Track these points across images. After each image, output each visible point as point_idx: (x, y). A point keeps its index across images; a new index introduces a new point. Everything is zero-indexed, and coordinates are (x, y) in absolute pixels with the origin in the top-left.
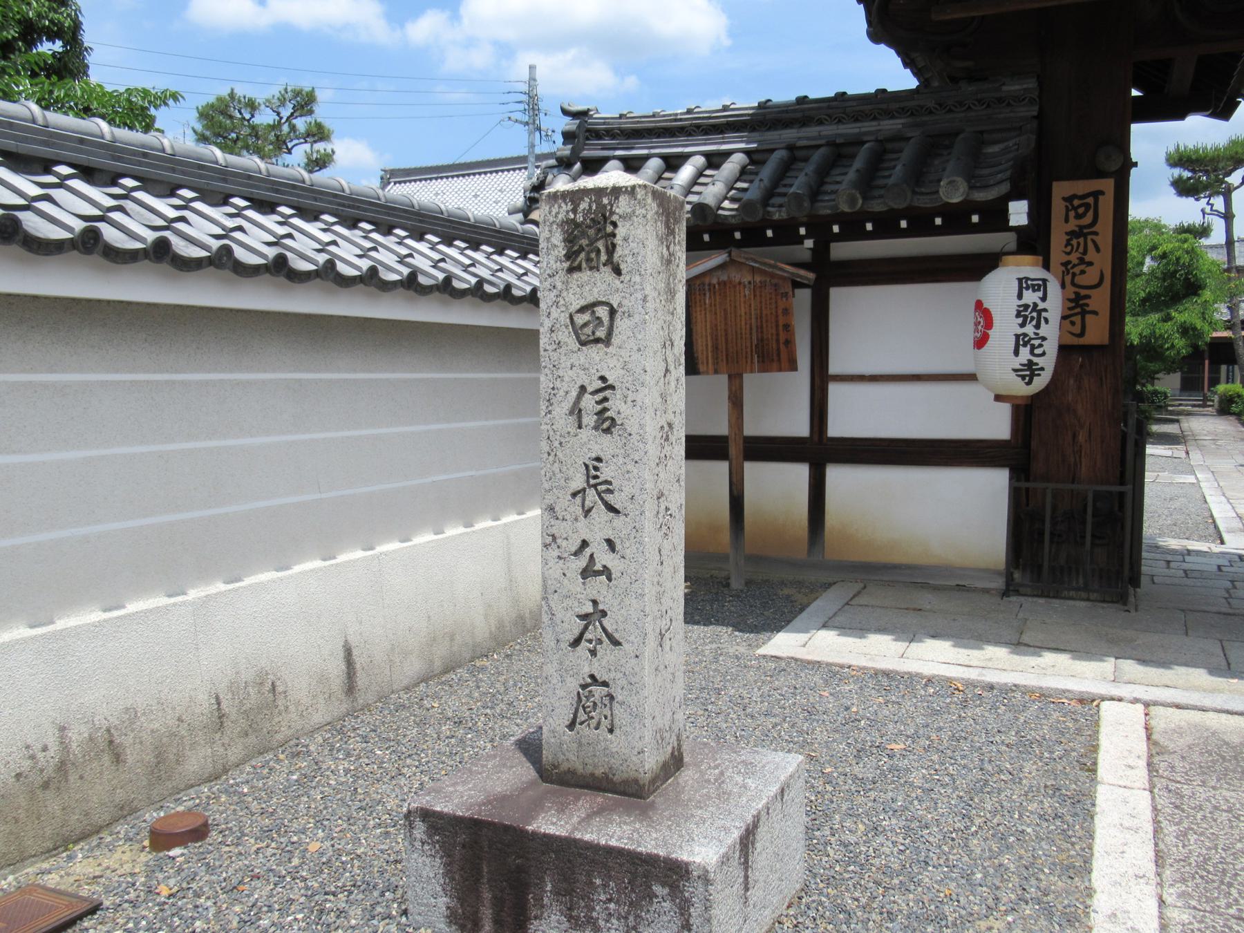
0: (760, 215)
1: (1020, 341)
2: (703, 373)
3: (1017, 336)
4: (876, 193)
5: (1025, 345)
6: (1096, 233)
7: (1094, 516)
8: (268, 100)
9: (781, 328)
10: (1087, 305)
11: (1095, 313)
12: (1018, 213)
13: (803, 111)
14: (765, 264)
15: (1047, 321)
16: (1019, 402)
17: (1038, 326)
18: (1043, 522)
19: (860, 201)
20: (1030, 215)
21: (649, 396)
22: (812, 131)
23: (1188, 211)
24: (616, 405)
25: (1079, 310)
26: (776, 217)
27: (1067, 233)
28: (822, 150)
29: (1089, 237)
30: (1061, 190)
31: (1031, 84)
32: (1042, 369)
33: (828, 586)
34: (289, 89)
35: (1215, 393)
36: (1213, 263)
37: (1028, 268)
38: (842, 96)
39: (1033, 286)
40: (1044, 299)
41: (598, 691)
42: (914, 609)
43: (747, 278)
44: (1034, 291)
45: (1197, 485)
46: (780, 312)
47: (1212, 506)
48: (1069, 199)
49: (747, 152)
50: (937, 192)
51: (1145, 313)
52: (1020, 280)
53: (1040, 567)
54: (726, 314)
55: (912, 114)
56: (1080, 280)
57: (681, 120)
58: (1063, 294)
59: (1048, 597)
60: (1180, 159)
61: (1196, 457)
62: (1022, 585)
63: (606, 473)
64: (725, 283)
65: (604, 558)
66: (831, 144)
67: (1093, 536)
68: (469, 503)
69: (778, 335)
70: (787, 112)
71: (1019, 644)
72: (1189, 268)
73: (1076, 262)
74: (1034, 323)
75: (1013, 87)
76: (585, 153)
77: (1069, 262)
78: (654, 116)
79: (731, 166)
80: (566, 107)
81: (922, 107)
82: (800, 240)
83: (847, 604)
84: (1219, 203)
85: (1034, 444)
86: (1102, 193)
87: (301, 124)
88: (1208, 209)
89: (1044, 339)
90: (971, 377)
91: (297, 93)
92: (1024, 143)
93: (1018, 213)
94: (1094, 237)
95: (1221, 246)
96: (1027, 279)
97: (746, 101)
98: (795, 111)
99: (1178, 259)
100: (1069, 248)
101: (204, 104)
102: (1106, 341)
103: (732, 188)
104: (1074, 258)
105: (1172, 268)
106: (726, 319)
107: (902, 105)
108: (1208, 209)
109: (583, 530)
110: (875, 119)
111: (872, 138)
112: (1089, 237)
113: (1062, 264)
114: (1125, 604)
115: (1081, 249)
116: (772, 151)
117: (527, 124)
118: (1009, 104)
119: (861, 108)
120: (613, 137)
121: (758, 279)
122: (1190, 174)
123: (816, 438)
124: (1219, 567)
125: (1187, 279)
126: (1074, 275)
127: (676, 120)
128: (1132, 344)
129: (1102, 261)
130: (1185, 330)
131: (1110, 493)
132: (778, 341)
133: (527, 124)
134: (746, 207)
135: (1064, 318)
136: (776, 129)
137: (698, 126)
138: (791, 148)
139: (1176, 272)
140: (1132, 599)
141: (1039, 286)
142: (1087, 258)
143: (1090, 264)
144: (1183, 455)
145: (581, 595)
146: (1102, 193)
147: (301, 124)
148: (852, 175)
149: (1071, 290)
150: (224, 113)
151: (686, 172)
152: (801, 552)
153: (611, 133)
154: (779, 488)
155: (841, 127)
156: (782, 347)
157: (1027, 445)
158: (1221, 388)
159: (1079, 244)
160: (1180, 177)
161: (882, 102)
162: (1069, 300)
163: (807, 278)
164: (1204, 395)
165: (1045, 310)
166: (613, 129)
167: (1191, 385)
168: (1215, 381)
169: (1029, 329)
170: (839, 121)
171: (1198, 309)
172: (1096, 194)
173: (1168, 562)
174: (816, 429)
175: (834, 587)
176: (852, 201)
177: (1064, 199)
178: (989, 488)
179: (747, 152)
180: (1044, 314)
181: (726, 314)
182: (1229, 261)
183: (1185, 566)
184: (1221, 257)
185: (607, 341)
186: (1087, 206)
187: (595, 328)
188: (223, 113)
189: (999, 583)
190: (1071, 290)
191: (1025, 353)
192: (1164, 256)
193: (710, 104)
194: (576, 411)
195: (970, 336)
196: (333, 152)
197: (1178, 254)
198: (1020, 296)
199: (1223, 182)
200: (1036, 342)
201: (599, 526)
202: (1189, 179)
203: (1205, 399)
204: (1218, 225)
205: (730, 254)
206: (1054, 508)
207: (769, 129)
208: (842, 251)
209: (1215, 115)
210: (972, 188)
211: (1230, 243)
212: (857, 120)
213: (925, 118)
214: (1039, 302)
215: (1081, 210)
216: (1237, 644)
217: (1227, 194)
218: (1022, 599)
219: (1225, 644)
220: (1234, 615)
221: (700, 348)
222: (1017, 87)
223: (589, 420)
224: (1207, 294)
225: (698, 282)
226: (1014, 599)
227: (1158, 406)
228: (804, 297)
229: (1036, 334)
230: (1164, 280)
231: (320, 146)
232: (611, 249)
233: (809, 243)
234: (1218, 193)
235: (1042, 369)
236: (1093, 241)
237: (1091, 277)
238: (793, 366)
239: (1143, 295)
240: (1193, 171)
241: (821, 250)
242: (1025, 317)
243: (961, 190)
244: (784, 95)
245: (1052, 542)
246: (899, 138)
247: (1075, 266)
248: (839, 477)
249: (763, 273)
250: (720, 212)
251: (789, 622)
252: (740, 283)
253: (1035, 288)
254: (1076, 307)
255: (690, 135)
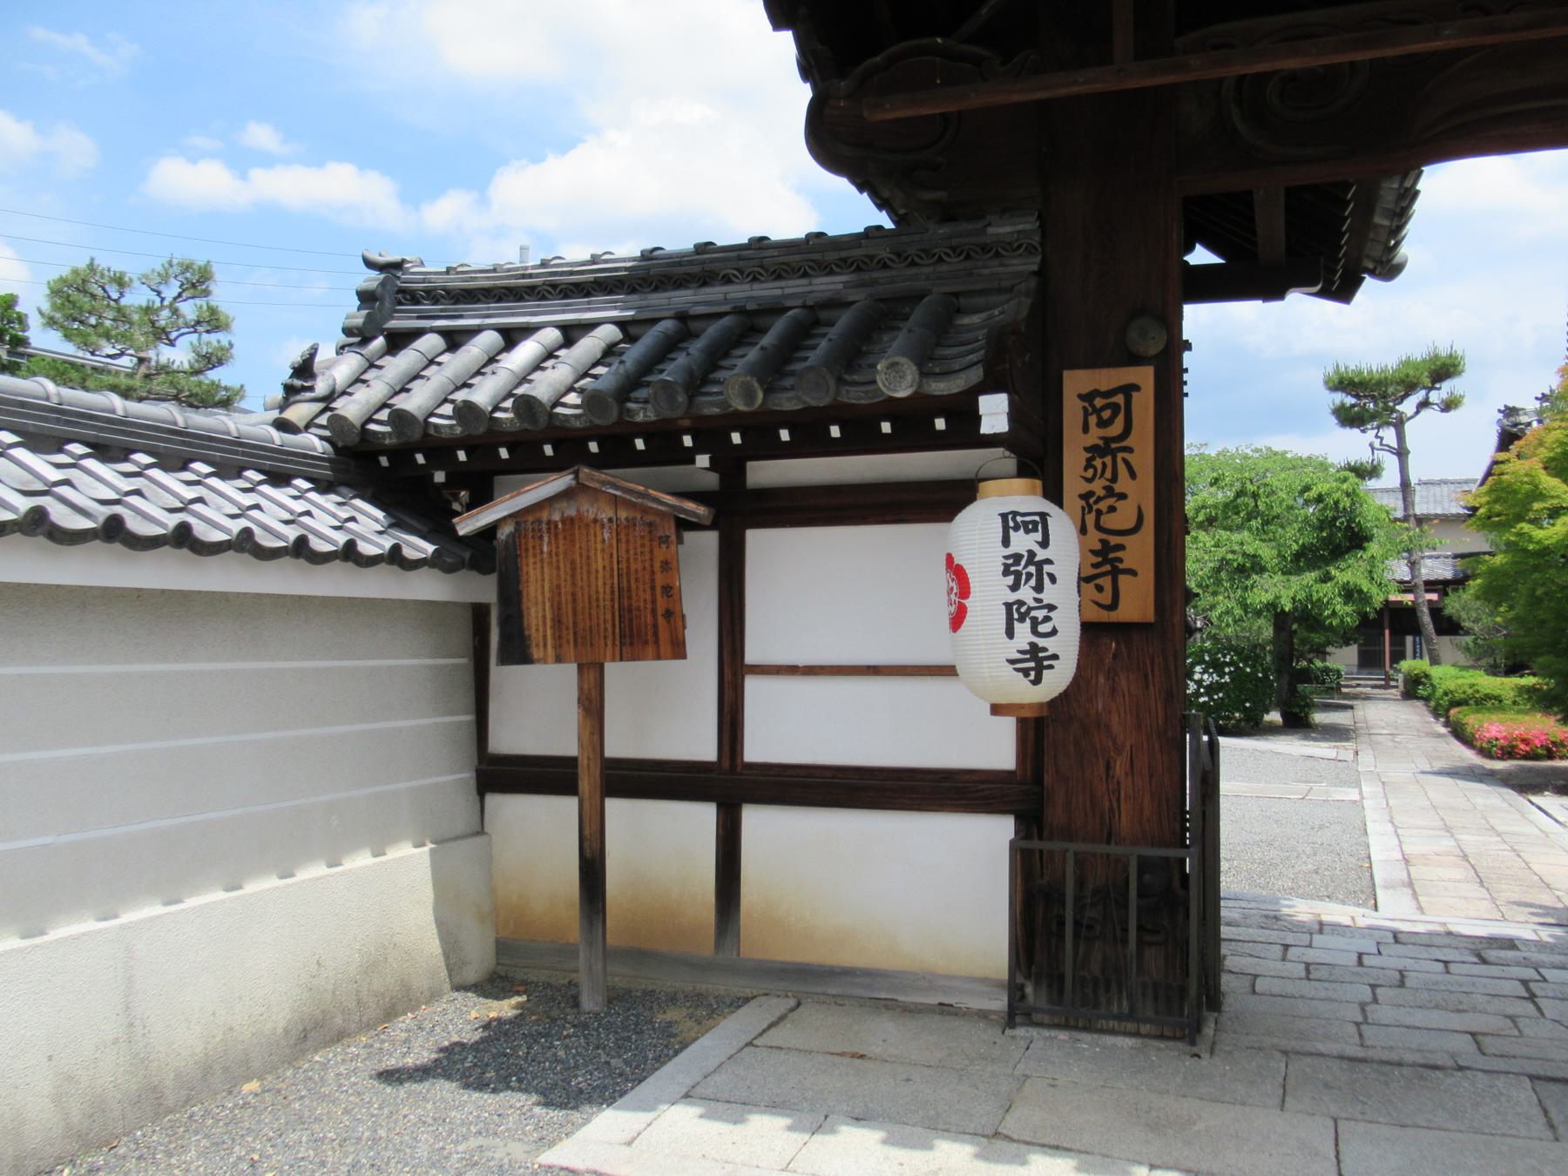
0: (614, 415)
1: (1014, 613)
2: (539, 661)
3: (1008, 606)
4: (788, 382)
5: (1022, 619)
6: (1129, 450)
7: (1140, 895)
8: (146, 276)
9: (658, 591)
10: (1120, 560)
11: (1133, 573)
12: (994, 413)
13: (703, 262)
14: (630, 492)
15: (1053, 579)
16: (1027, 714)
17: (1039, 588)
18: (1063, 904)
19: (760, 395)
20: (1013, 416)
22: (715, 292)
23: (1354, 445)
25: (1108, 567)
26: (640, 418)
27: (1086, 449)
28: (726, 321)
29: (1120, 455)
30: (1076, 382)
31: (1028, 224)
32: (1055, 657)
33: (740, 1002)
34: (175, 262)
35: (1399, 671)
36: (1381, 508)
37: (1018, 498)
38: (760, 243)
39: (1025, 524)
40: (1044, 544)
42: (853, 1056)
43: (606, 514)
44: (1027, 531)
45: (1358, 805)
46: (657, 565)
47: (1372, 840)
48: (1088, 397)
49: (621, 324)
50: (875, 382)
51: (1298, 571)
52: (1004, 516)
53: (1061, 977)
54: (573, 569)
55: (859, 269)
56: (1109, 521)
57: (530, 276)
58: (1081, 544)
59: (1076, 1028)
60: (1341, 382)
61: (1366, 758)
62: (1038, 1010)
64: (572, 520)
66: (739, 311)
67: (1140, 928)
68: (281, 847)
69: (654, 601)
70: (680, 264)
71: (996, 1134)
72: (1351, 514)
73: (1101, 493)
74: (1033, 582)
75: (1002, 229)
76: (393, 324)
77: (1090, 494)
78: (494, 270)
79: (590, 345)
80: (374, 256)
81: (871, 258)
82: (688, 457)
83: (750, 1044)
84: (1389, 435)
85: (1048, 779)
86: (1137, 388)
87: (189, 309)
88: (1377, 443)
89: (1051, 608)
90: (948, 671)
91: (187, 268)
92: (1012, 309)
93: (994, 413)
94: (1126, 455)
95: (1393, 490)
96: (1015, 514)
97: (626, 250)
98: (690, 263)
99: (1336, 503)
100: (1090, 473)
101: (57, 277)
102: (1150, 617)
103: (586, 375)
104: (1098, 487)
105: (1330, 514)
106: (573, 576)
107: (844, 254)
108: (1377, 443)
110: (805, 275)
111: (799, 302)
112: (1120, 455)
113: (1081, 496)
114: (1193, 1043)
115: (1108, 474)
116: (654, 321)
118: (998, 255)
119: (786, 259)
120: (436, 301)
121: (623, 514)
122: (1353, 401)
123: (726, 764)
124: (1360, 956)
125: (1349, 528)
126: (1099, 513)
127: (524, 276)
128: (1283, 611)
129: (1140, 492)
130: (1349, 593)
131: (1167, 859)
132: (654, 611)
134: (592, 400)
135: (1083, 580)
136: (665, 290)
137: (554, 286)
138: (682, 317)
139: (1335, 519)
140: (1209, 1030)
141: (1035, 523)
142: (1118, 488)
143: (1122, 496)
144: (1349, 756)
146: (1137, 388)
147: (189, 309)
148: (753, 354)
149: (1094, 537)
150: (82, 290)
151: (527, 350)
153: (432, 295)
154: (662, 844)
155: (756, 286)
156: (661, 620)
157: (1038, 779)
158: (1406, 665)
159: (1104, 465)
160: (1343, 405)
161: (816, 253)
162: (1093, 552)
163: (695, 514)
164: (1386, 673)
165: (1049, 562)
166: (435, 289)
167: (1370, 661)
168: (1398, 656)
169: (1026, 594)
170: (755, 279)
171: (1364, 566)
172: (1129, 390)
173: (1286, 947)
174: (726, 749)
175: (754, 1003)
176: (749, 395)
177: (1081, 397)
178: (989, 838)
179: (621, 324)
180: (1047, 568)
181: (573, 569)
182: (1406, 509)
183: (1311, 955)
184: (1395, 505)
186: (1115, 408)
188: (82, 290)
189: (1000, 1003)
190: (1094, 537)
191: (1023, 630)
192: (1320, 499)
193: (575, 253)
195: (945, 613)
196: (231, 345)
197: (1336, 496)
198: (1006, 542)
199: (1393, 410)
200: (1040, 614)
202: (1353, 406)
203: (1388, 679)
204: (1390, 463)
205: (576, 474)
206: (1081, 883)
207: (656, 289)
208: (764, 473)
209: (1325, 293)
210: (924, 374)
211: (1405, 485)
212: (779, 277)
213: (875, 275)
214: (1036, 548)
215: (1106, 414)
216: (1362, 1127)
217: (1399, 425)
218: (1033, 1032)
219: (1342, 1126)
220: (1364, 1061)
221: (534, 622)
222: (1008, 229)
224: (1373, 548)
225: (531, 519)
226: (1021, 1032)
227: (1330, 685)
228: (706, 544)
229: (1037, 600)
230: (1321, 529)
231: (213, 338)
233: (703, 460)
234: (1388, 424)
235: (1055, 657)
236: (1124, 460)
237: (1123, 517)
239: (1295, 547)
240: (1357, 396)
242: (1018, 575)
243: (909, 378)
244: (678, 241)
245: (1077, 936)
246: (836, 303)
247: (1099, 499)
248: (762, 825)
249: (633, 506)
250: (559, 410)
251: (623, 1094)
252: (595, 521)
253: (1029, 528)
254: (1103, 565)
255: (544, 298)
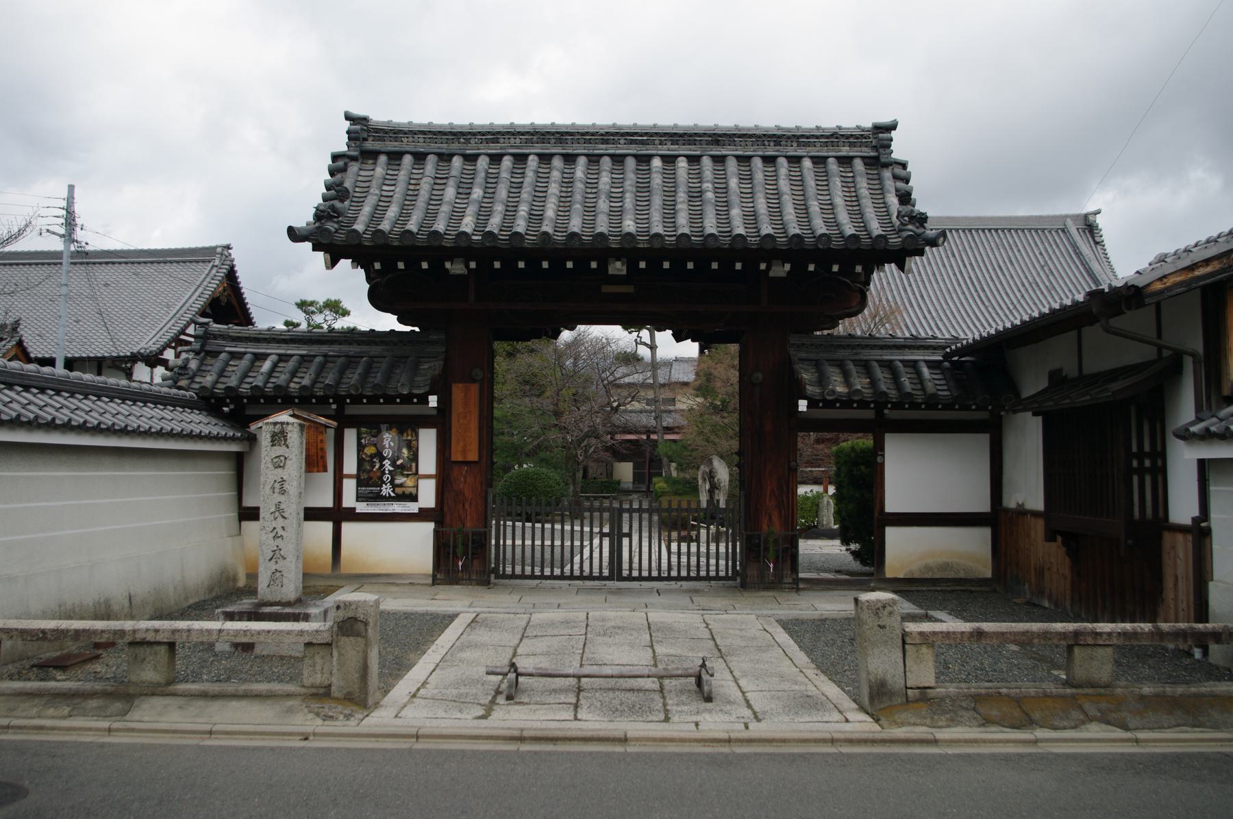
12: (433, 401)
21: (295, 483)
22: (336, 348)
24: (286, 486)
41: (278, 574)
63: (282, 506)
65: (281, 532)
85: (445, 509)
93: (433, 401)
109: (274, 524)
116: (315, 356)
117: (62, 236)
133: (62, 236)
138: (325, 356)
145: (273, 544)
151: (267, 366)
152: (328, 570)
185: (283, 467)
187: (279, 463)
189: (430, 581)
194: (273, 488)
201: (280, 522)
223: (277, 490)
232: (286, 440)
233: (334, 406)
238: (325, 470)
241: (341, 409)
248: (347, 528)
